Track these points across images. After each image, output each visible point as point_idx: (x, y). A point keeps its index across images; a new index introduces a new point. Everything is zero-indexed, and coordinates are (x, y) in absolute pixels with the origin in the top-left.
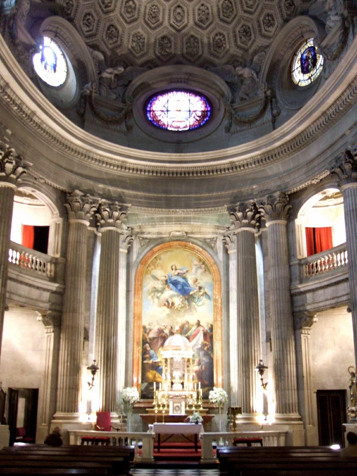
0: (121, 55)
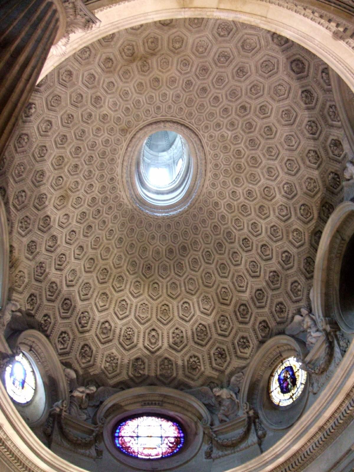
0: (94, 375)
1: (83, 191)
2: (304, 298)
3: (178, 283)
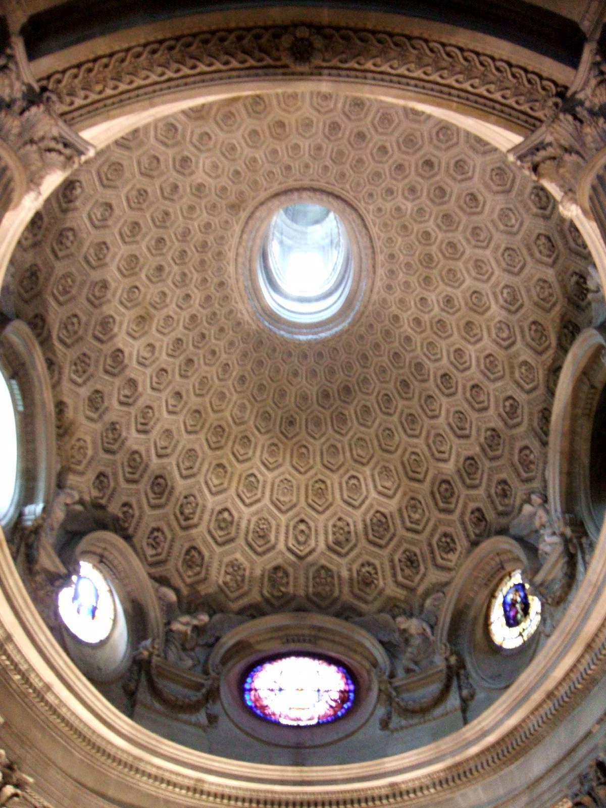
0: (206, 595)
1: (174, 306)
2: (539, 475)
3: (339, 445)
